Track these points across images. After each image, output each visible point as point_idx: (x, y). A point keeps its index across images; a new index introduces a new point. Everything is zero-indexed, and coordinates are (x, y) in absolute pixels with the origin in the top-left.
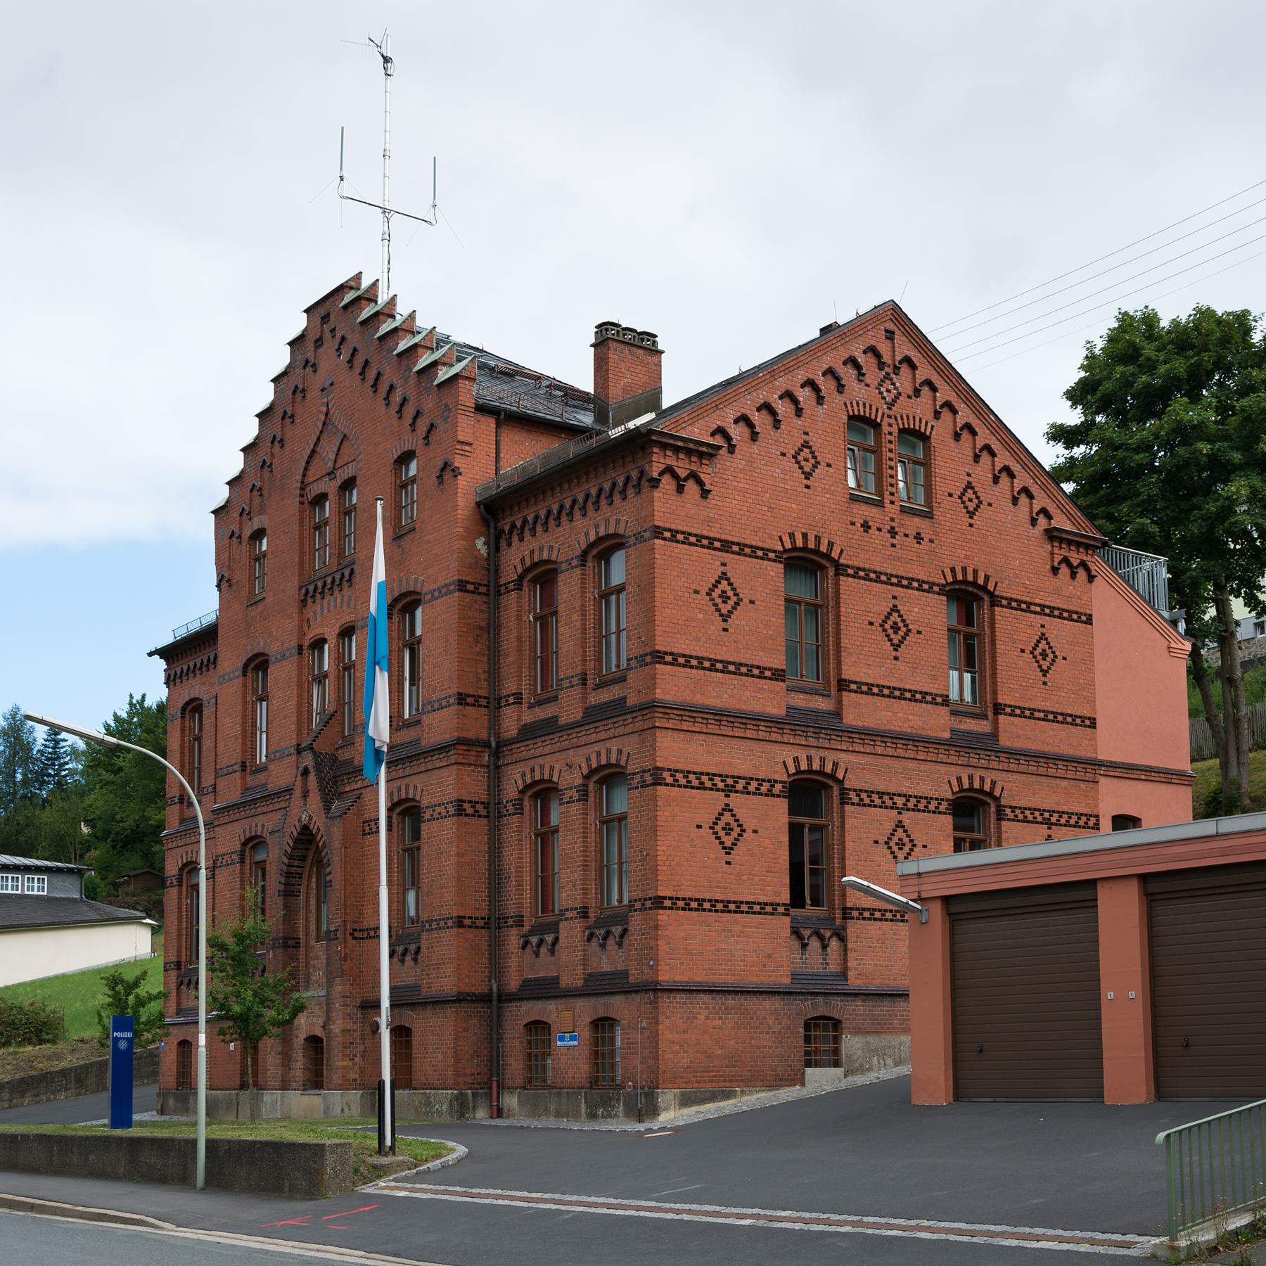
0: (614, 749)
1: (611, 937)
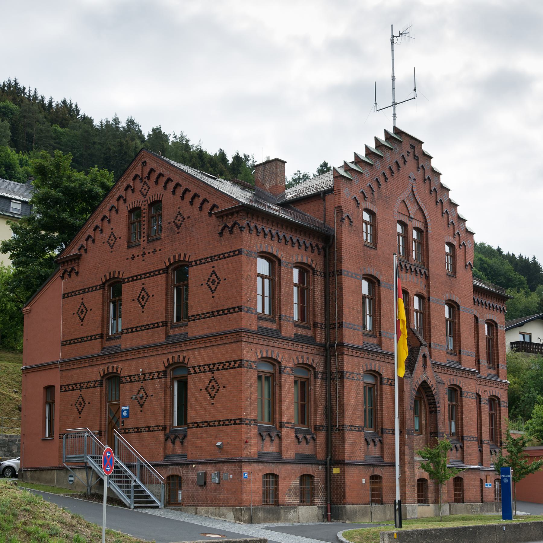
0: (115, 366)
1: (169, 439)
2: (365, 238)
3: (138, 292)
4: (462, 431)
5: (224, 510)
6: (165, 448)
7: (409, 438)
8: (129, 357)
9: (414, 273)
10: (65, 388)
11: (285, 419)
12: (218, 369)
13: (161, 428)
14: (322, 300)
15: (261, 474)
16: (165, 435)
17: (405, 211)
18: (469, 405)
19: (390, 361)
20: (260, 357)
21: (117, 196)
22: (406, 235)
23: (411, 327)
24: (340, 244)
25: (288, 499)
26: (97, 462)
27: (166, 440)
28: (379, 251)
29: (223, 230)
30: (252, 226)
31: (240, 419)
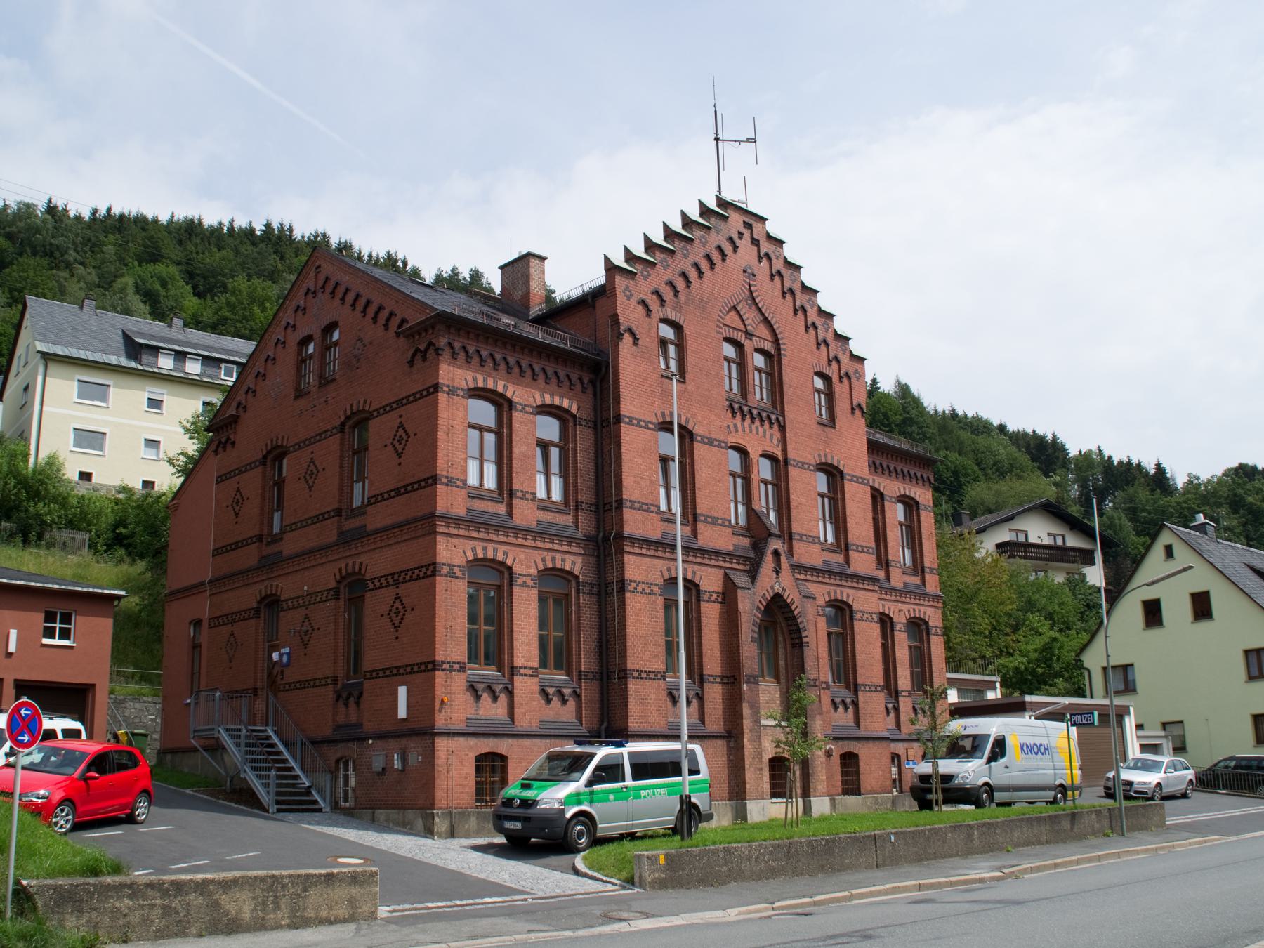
3: (305, 465)
5: (410, 814)
7: (749, 689)
8: (291, 569)
10: (215, 622)
11: (518, 662)
12: (405, 581)
13: (329, 681)
14: (592, 466)
15: (472, 755)
16: (336, 692)
18: (867, 638)
19: (668, 555)
20: (470, 557)
21: (284, 323)
22: (741, 364)
23: (755, 506)
24: (616, 374)
26: (232, 737)
27: (337, 700)
29: (414, 356)
30: (457, 345)
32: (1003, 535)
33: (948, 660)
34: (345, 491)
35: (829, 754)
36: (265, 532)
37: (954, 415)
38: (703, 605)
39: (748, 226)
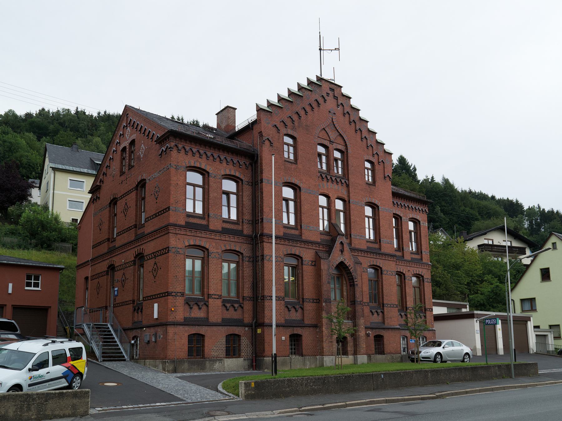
2: (367, 179)
4: (383, 300)
5: (158, 362)
6: (133, 317)
9: (335, 183)
10: (94, 277)
14: (250, 203)
15: (187, 335)
16: (133, 307)
17: (326, 137)
24: (261, 160)
25: (214, 354)
28: (300, 166)
30: (180, 146)
31: (167, 292)
32: (482, 241)
33: (434, 292)
34: (138, 216)
35: (368, 335)
36: (111, 237)
37: (470, 192)
38: (304, 266)
39: (332, 90)
